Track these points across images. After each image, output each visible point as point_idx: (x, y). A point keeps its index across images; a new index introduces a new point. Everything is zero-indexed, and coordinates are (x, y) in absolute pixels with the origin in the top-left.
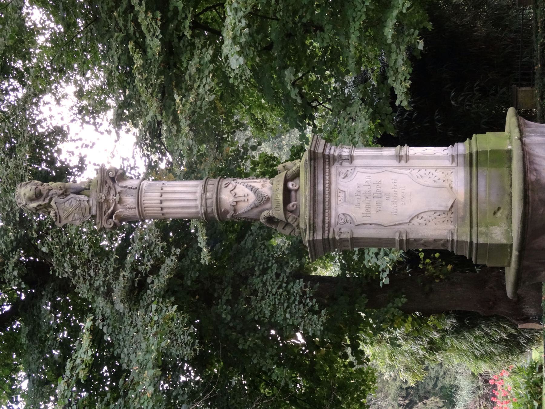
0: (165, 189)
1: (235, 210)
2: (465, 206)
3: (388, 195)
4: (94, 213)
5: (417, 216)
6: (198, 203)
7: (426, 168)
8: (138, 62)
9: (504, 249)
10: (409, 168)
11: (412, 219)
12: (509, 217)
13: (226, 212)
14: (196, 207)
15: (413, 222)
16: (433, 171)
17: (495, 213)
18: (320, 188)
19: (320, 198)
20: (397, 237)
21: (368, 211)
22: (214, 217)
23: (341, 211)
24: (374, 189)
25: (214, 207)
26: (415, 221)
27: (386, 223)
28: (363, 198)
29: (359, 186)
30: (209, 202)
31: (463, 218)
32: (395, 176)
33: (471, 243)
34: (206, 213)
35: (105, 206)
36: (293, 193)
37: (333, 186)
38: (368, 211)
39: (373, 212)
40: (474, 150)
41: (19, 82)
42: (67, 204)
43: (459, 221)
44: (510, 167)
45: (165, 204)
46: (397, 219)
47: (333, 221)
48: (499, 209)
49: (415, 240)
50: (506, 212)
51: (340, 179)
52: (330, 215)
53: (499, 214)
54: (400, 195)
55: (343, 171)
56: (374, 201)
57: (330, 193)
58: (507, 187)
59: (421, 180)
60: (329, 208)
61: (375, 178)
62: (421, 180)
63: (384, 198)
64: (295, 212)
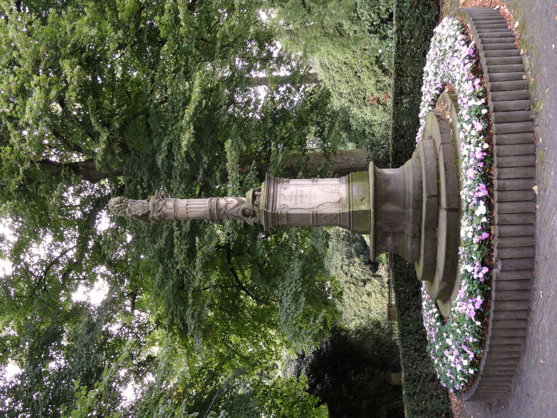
0: (189, 203)
1: (226, 208)
2: (346, 200)
3: (307, 196)
4: (150, 209)
5: (322, 205)
6: (207, 205)
7: (326, 185)
8: (177, 233)
9: (367, 212)
10: (318, 185)
11: (319, 206)
12: (369, 202)
13: (221, 209)
14: (205, 207)
15: (320, 207)
16: (330, 186)
17: (362, 200)
18: (272, 191)
19: (271, 196)
20: (311, 213)
21: (296, 203)
22: (214, 214)
23: (282, 203)
24: (299, 193)
25: (215, 206)
26: (320, 207)
27: (306, 208)
28: (294, 197)
29: (292, 192)
30: (212, 204)
31: (345, 205)
32: (310, 188)
33: (349, 212)
34: (210, 210)
35: (156, 206)
36: (257, 197)
37: (278, 193)
38: (296, 203)
39: (299, 202)
40: (351, 210)
41: (102, 373)
42: (136, 205)
43: (344, 206)
44: (368, 181)
45: (189, 206)
46: (311, 206)
47: (277, 207)
48: (364, 198)
49: (320, 214)
50: (367, 200)
51: (282, 190)
52: (276, 204)
53: (364, 200)
54: (313, 196)
55: (285, 186)
56: (299, 199)
57: (276, 195)
58: (368, 190)
59: (324, 190)
60: (276, 201)
61: (300, 189)
62: (324, 190)
63: (305, 197)
64: (257, 205)
